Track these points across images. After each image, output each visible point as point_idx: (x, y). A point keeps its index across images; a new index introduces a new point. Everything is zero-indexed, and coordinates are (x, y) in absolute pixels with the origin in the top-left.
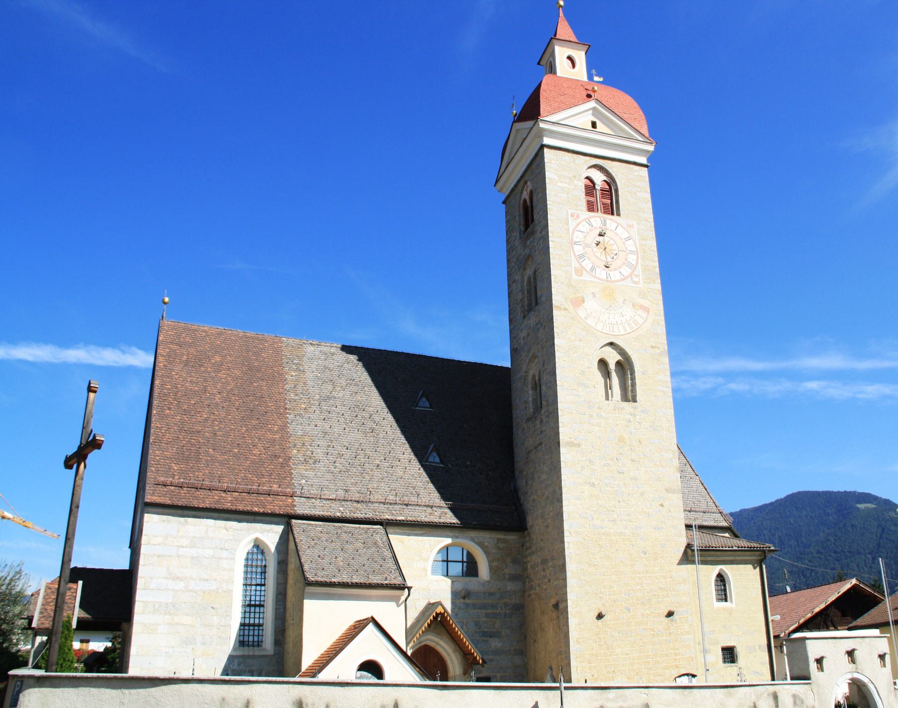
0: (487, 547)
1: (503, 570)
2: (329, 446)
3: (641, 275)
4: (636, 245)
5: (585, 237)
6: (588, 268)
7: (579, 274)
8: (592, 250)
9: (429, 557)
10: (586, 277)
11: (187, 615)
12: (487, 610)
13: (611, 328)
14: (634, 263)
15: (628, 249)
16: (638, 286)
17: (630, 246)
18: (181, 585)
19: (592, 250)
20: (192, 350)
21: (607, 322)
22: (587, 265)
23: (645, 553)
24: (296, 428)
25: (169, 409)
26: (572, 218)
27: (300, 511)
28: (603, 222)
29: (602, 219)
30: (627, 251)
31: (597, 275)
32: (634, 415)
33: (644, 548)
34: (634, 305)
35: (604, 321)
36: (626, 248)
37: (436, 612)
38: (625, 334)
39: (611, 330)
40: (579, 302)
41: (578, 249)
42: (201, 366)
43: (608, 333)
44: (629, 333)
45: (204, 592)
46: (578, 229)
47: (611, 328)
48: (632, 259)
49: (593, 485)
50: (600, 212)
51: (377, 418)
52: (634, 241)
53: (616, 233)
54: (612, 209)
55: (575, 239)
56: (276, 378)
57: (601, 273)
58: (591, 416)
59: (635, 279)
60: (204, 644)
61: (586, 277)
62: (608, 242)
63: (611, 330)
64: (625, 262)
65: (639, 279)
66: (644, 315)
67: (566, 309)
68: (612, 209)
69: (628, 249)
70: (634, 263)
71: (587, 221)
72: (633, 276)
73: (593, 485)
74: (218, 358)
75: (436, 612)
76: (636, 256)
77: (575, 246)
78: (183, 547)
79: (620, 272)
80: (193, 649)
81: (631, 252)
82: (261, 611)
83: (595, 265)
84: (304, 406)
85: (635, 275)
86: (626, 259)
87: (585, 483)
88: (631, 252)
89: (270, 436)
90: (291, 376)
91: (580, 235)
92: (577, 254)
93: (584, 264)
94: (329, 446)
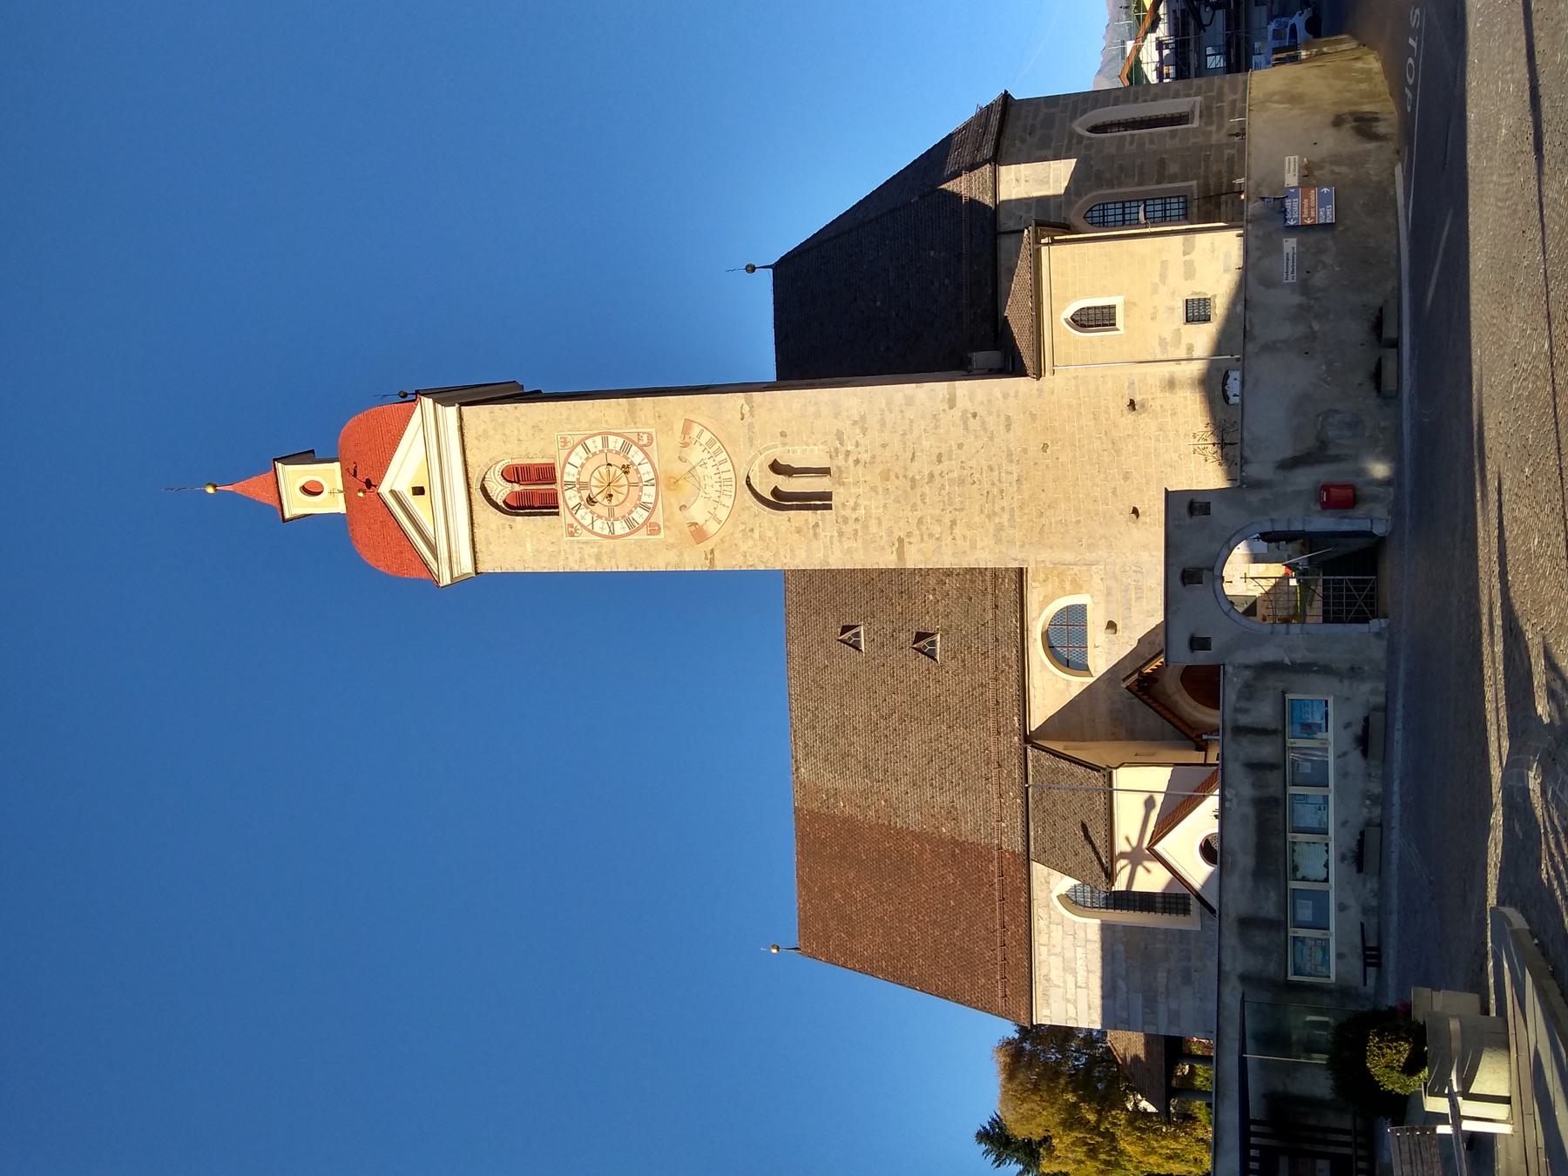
0: (1045, 597)
1: (1076, 574)
2: (931, 785)
3: (639, 430)
4: (595, 435)
5: (600, 517)
6: (646, 514)
7: (657, 528)
8: (616, 506)
9: (1064, 679)
10: (658, 517)
11: (1155, 978)
12: (1131, 599)
13: (726, 483)
14: (621, 441)
15: (601, 448)
16: (654, 435)
17: (595, 444)
18: (1121, 983)
19: (616, 506)
20: (832, 924)
21: (719, 489)
22: (640, 516)
23: (1045, 447)
24: (913, 820)
25: (911, 968)
26: (576, 534)
27: (1019, 849)
28: (570, 486)
29: (565, 488)
30: (606, 451)
31: (652, 500)
32: (848, 453)
33: (1038, 446)
34: (685, 445)
35: (718, 494)
36: (601, 451)
37: (1138, 691)
38: (732, 462)
39: (729, 483)
40: (698, 533)
41: (620, 527)
42: (851, 918)
43: (734, 486)
44: (728, 455)
45: (1128, 958)
46: (590, 527)
47: (726, 483)
48: (615, 443)
49: (953, 523)
50: (553, 486)
51: (885, 711)
52: (587, 438)
53: (582, 465)
54: (546, 474)
55: (606, 532)
56: (850, 828)
57: (649, 494)
58: (857, 520)
59: (645, 440)
60: (1189, 959)
61: (658, 517)
62: (598, 480)
63: (729, 483)
64: (638, 502)
65: (644, 433)
66: (696, 429)
67: (712, 552)
68: (546, 474)
69: (601, 448)
70: (621, 441)
71: (574, 512)
72: (641, 443)
73: (953, 523)
74: (837, 895)
75: (1138, 691)
76: (610, 437)
77: (616, 533)
78: (1076, 982)
79: (640, 464)
80: (1195, 971)
81: (605, 442)
82: (1117, 223)
83: (638, 502)
84: (883, 802)
85: (639, 439)
86: (617, 453)
87: (951, 534)
88: (605, 442)
89: (927, 856)
90: (843, 807)
91: (598, 524)
92: (627, 530)
93: (641, 521)
94: (931, 785)
